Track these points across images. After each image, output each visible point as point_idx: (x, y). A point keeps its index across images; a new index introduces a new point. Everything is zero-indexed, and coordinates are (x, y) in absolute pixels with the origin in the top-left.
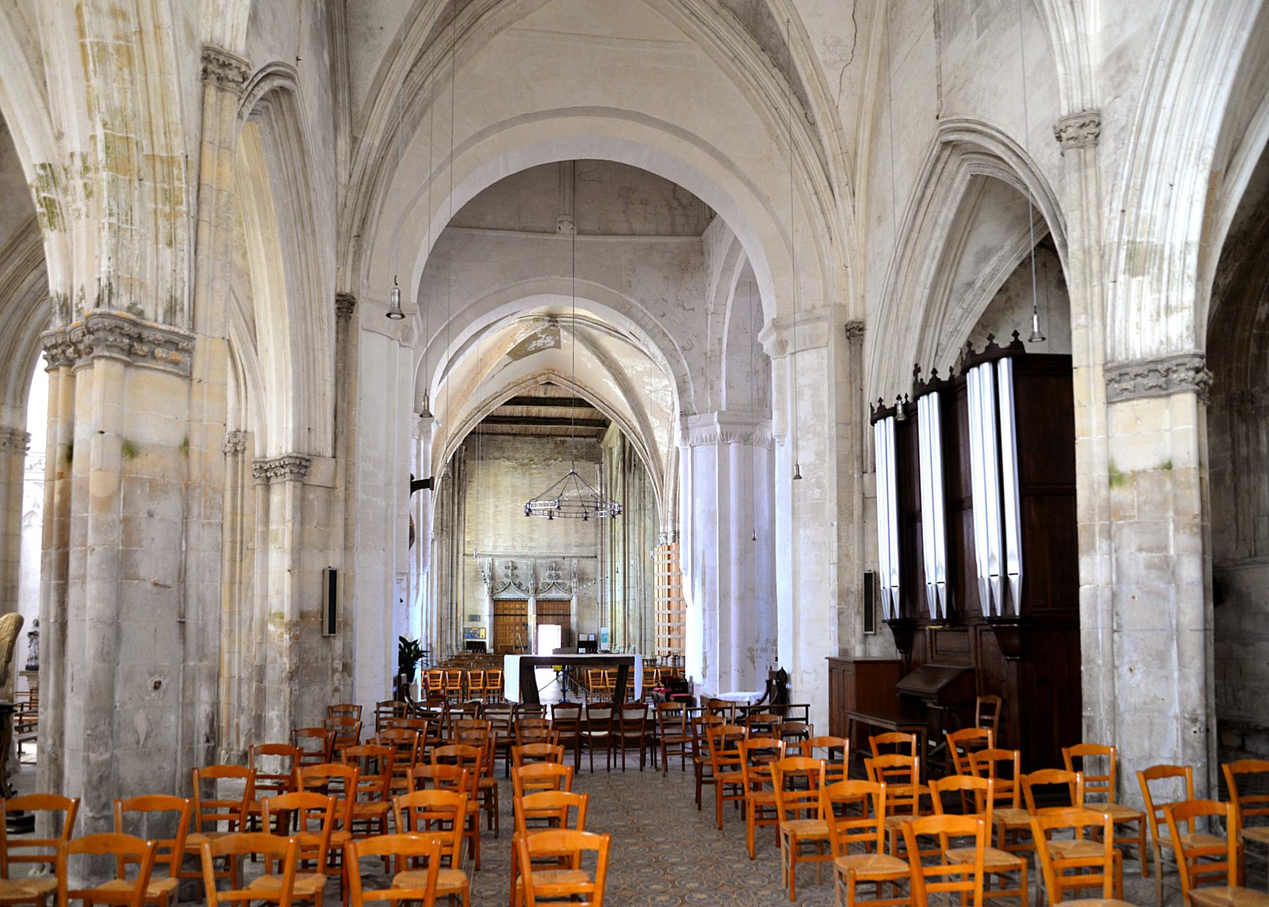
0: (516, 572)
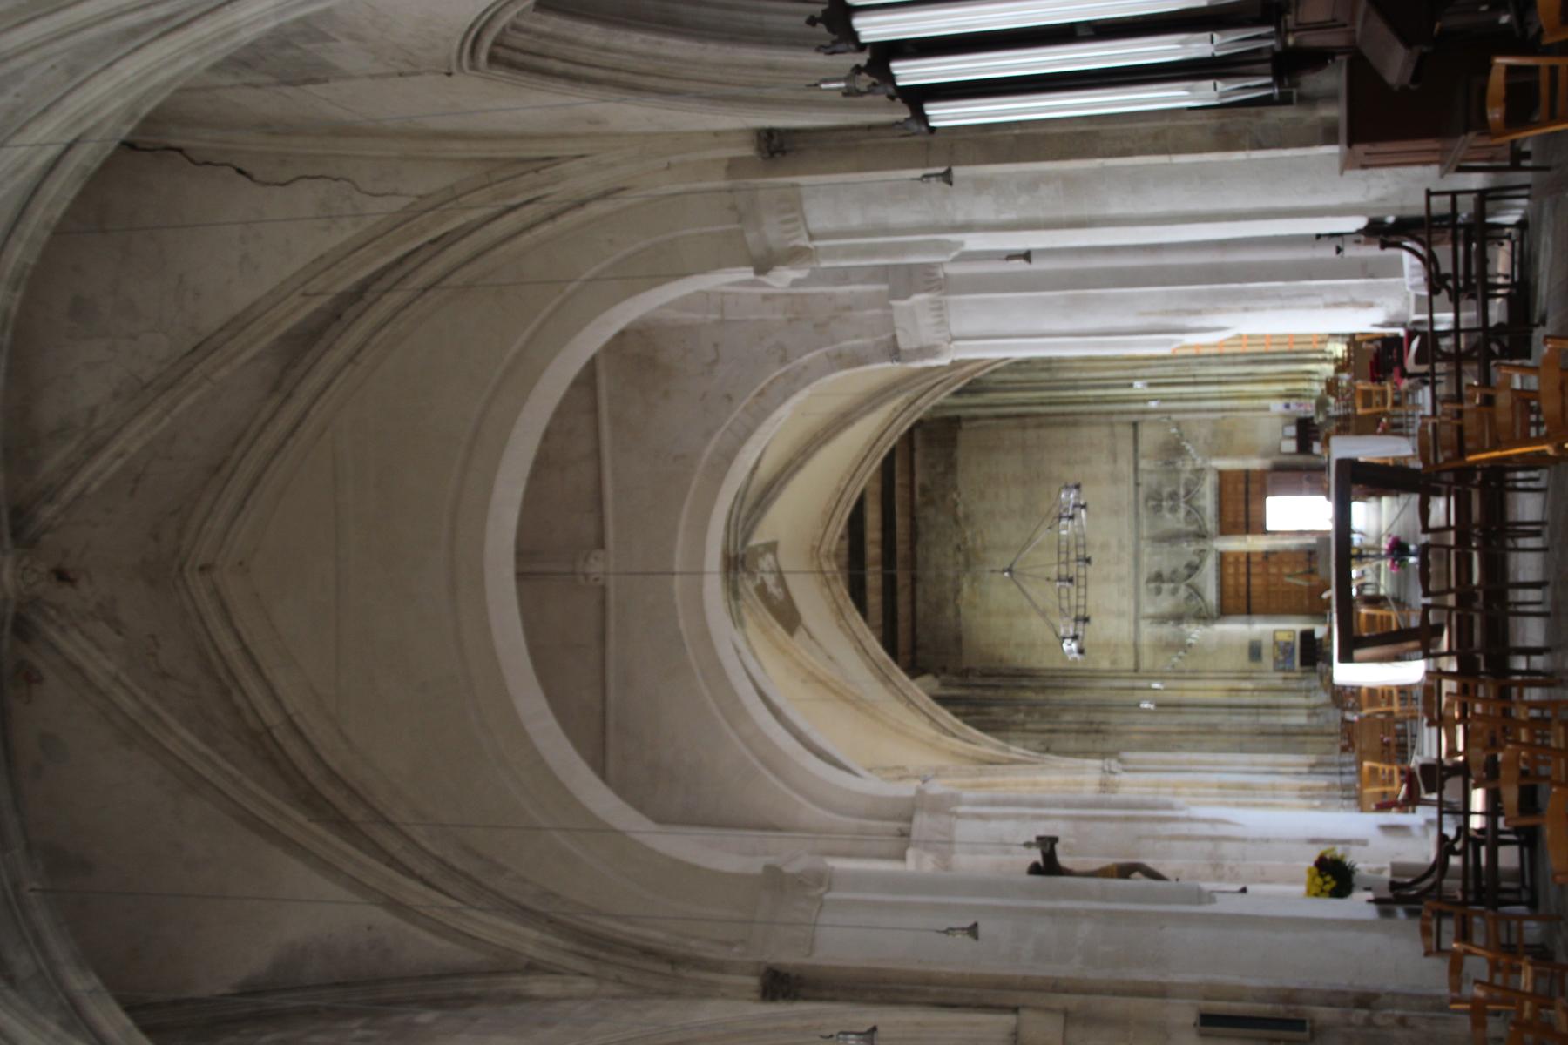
0: (1166, 573)
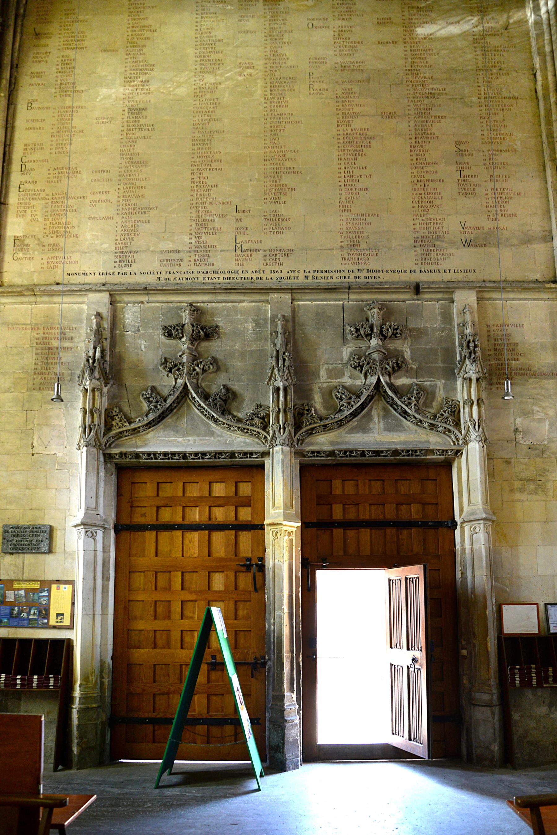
0: (214, 347)
